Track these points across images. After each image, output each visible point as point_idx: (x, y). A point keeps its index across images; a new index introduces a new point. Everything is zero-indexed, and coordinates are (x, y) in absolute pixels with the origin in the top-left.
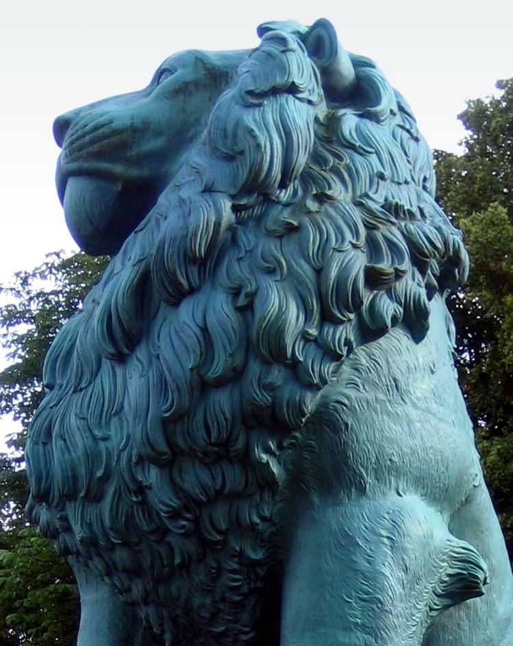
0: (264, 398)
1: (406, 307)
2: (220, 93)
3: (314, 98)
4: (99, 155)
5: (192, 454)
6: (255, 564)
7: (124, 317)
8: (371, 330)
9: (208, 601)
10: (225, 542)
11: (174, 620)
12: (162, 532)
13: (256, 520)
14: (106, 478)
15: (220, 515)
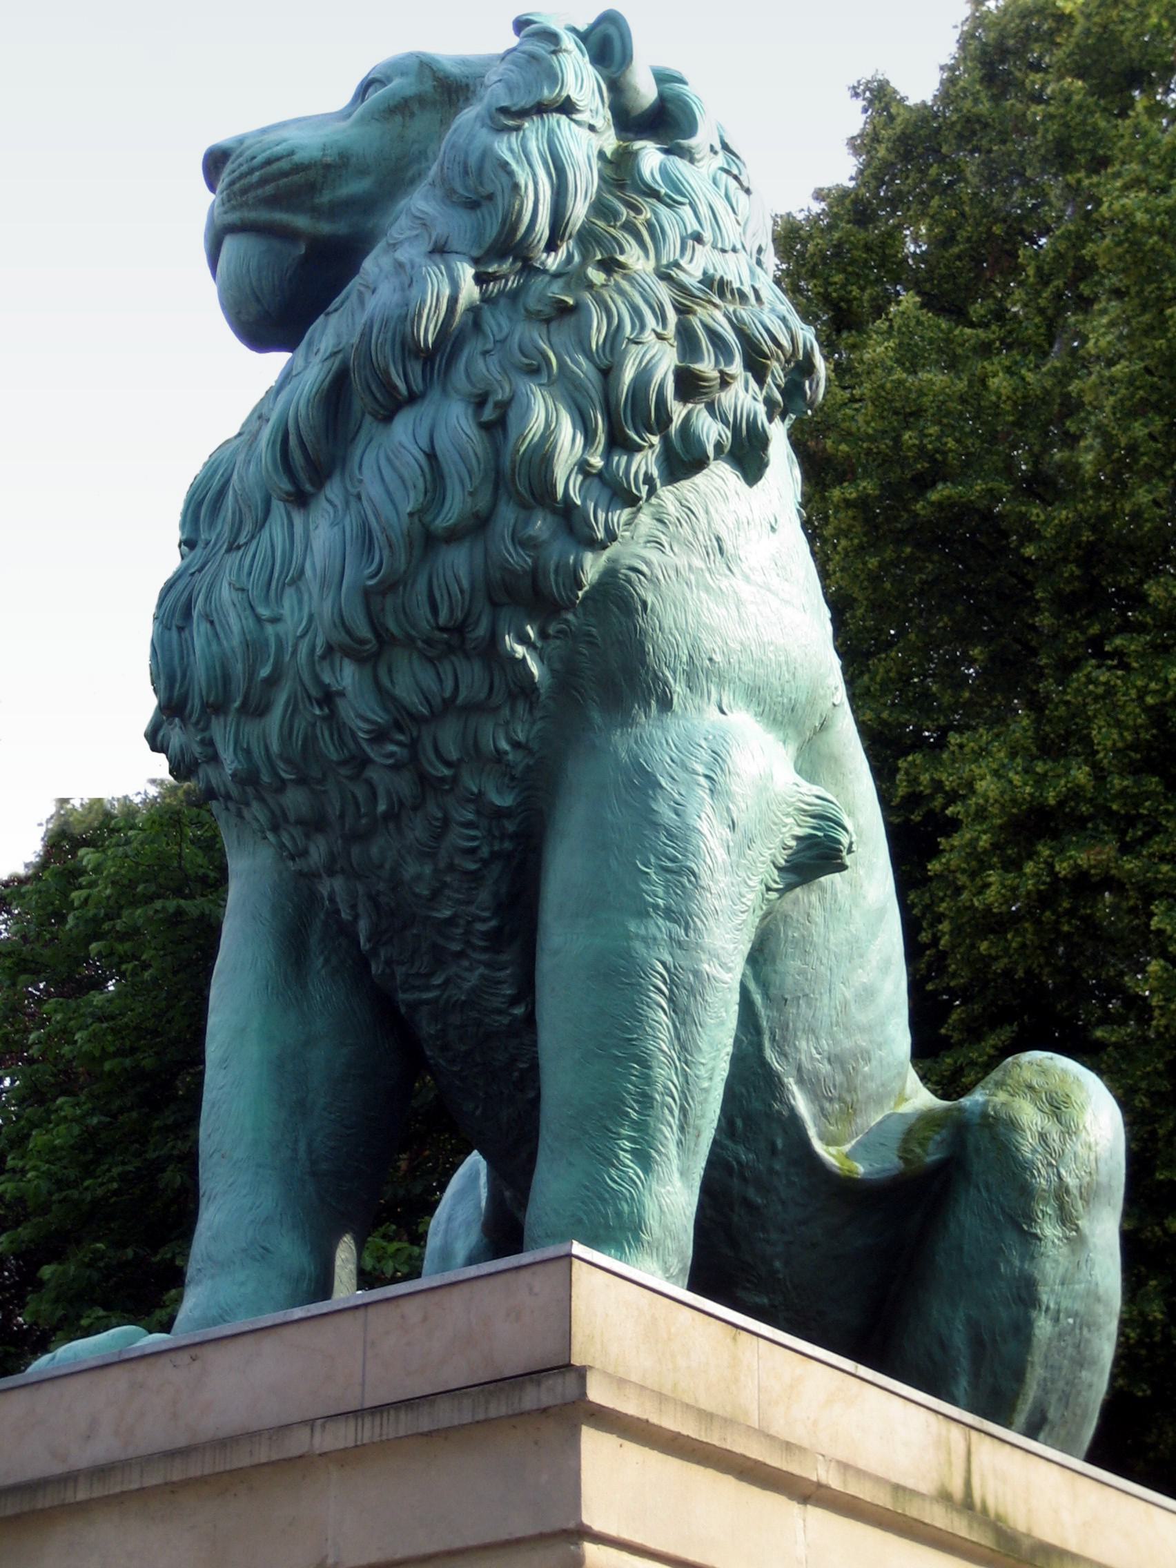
6: (500, 814)
8: (684, 461)
9: (428, 870)
10: (455, 780)
11: (373, 898)
13: (504, 746)
14: (272, 682)
15: (449, 737)
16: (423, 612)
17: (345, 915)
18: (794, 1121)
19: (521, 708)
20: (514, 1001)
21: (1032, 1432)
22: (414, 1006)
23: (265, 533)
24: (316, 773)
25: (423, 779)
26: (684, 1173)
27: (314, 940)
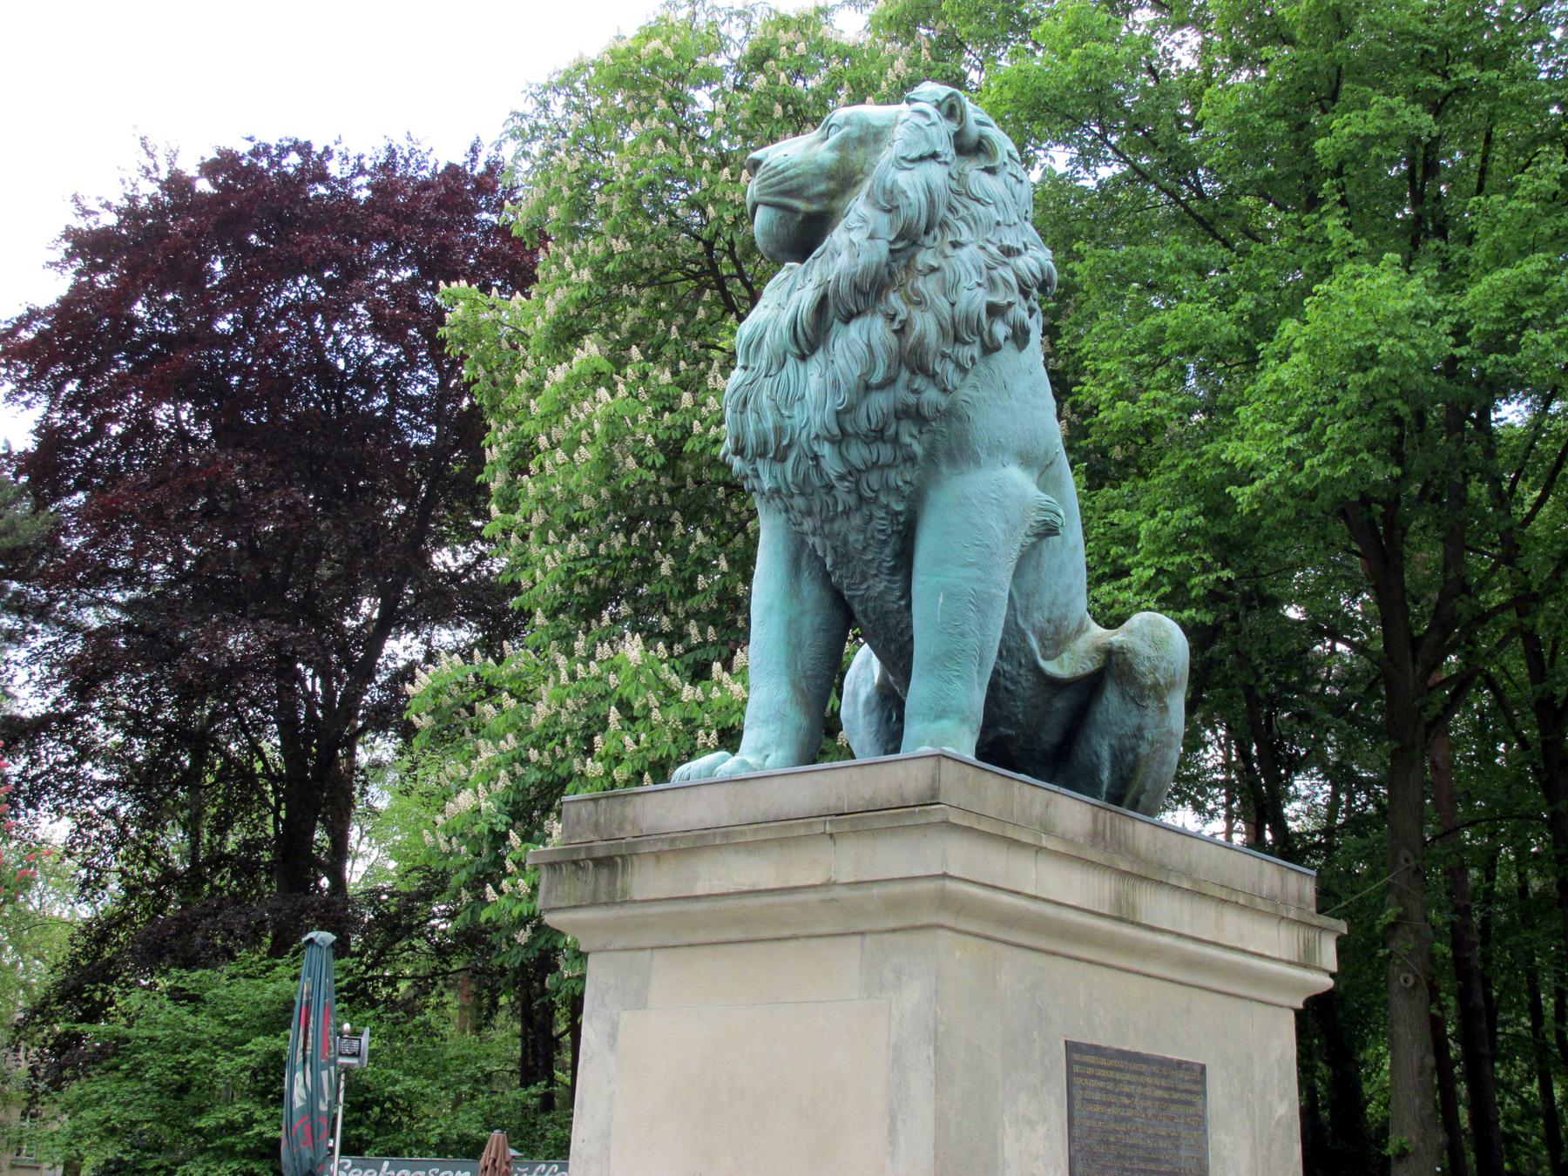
0: (911, 399)
1: (1014, 327)
2: (878, 152)
3: (948, 159)
4: (784, 193)
5: (857, 435)
6: (898, 514)
7: (808, 331)
8: (990, 348)
9: (861, 537)
10: (876, 498)
11: (834, 549)
12: (830, 488)
13: (900, 483)
14: (790, 446)
15: (874, 479)
16: (863, 423)
17: (820, 553)
18: (1031, 651)
19: (909, 464)
20: (901, 598)
21: (1133, 807)
22: (853, 597)
23: (784, 372)
24: (809, 490)
25: (861, 498)
26: (980, 685)
27: (804, 563)
